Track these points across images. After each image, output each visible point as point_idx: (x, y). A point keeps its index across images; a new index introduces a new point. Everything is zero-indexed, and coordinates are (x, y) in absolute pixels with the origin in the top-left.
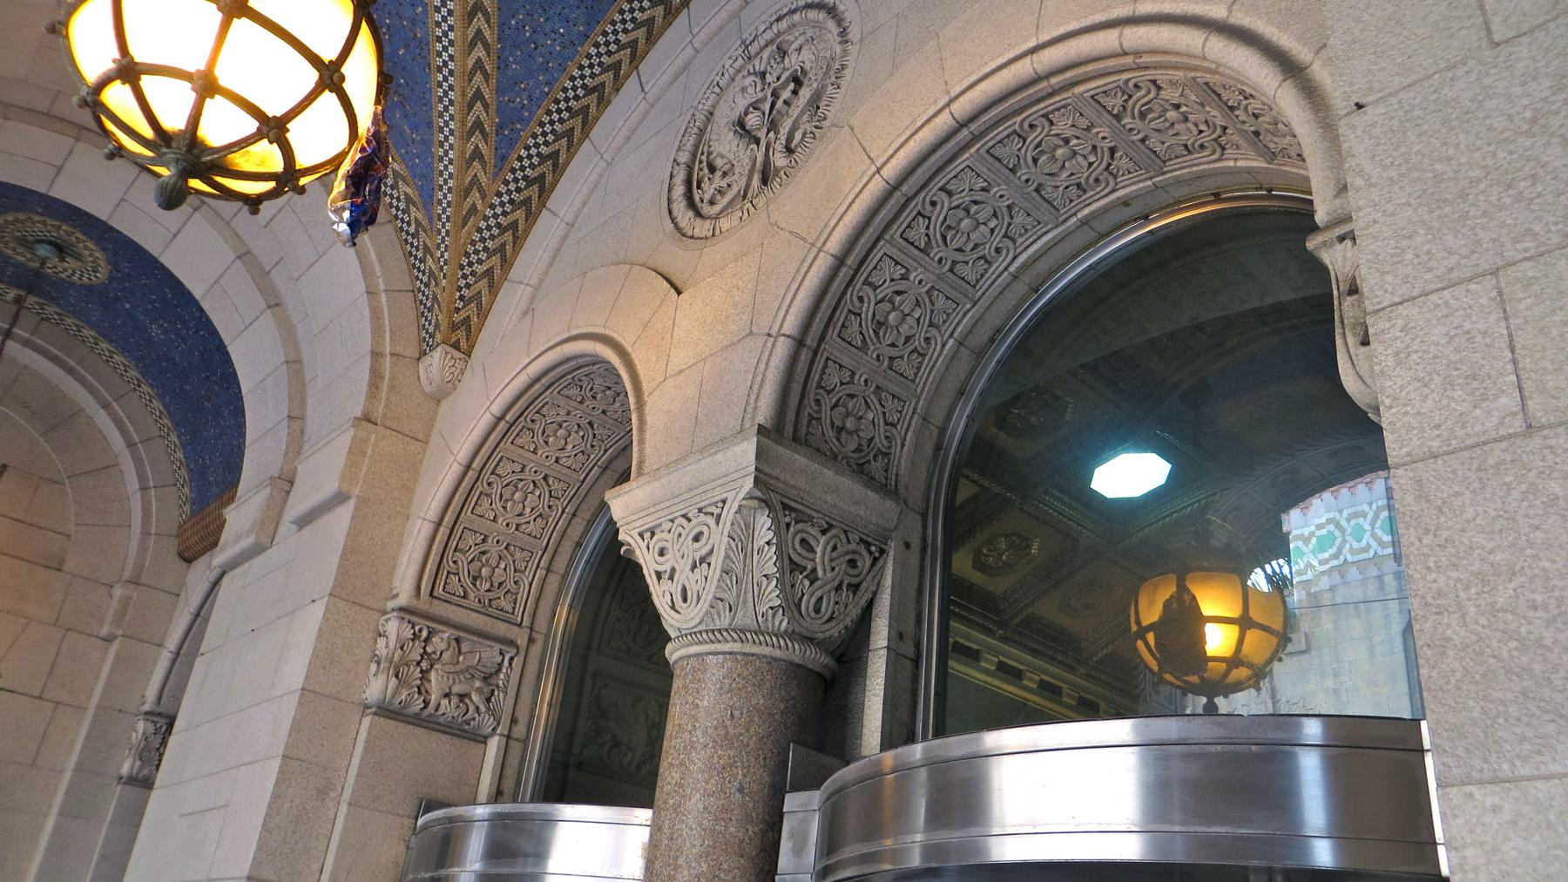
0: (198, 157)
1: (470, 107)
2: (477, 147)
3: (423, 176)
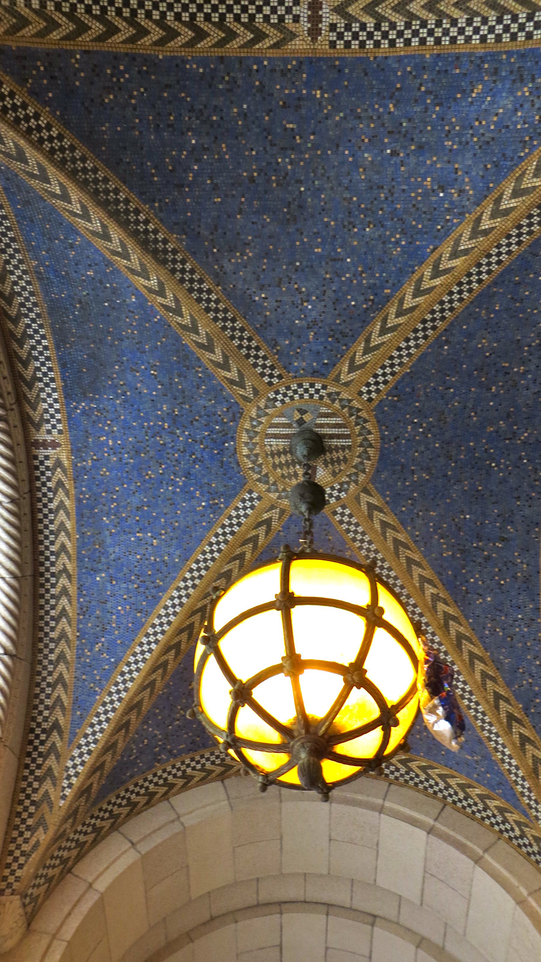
0: (316, 734)
1: (497, 707)
2: (521, 734)
3: (500, 784)
